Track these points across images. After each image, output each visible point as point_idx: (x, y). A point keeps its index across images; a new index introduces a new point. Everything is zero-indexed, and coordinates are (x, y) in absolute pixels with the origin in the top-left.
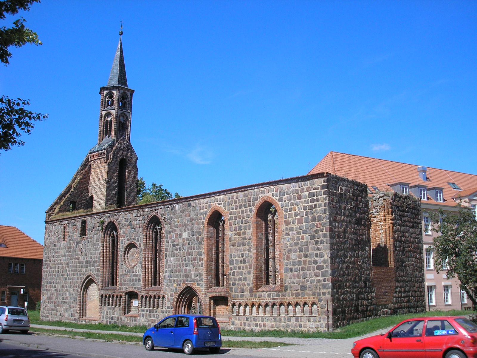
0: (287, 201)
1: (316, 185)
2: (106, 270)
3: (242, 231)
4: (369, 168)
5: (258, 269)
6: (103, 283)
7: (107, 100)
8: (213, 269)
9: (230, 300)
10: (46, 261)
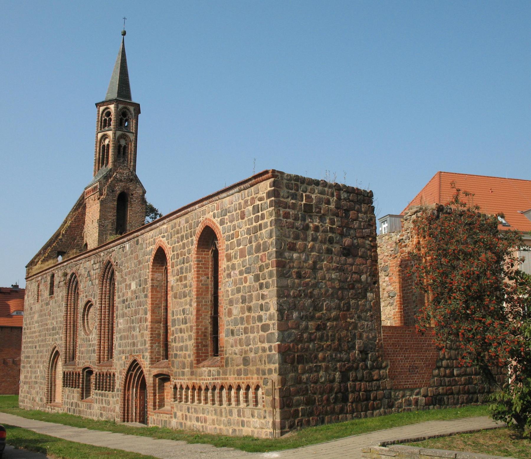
0: (229, 224)
1: (262, 193)
2: (70, 338)
3: (183, 275)
4: (495, 191)
5: (200, 333)
6: (66, 356)
7: (103, 119)
8: (162, 334)
9: (172, 380)
10: (25, 329)
